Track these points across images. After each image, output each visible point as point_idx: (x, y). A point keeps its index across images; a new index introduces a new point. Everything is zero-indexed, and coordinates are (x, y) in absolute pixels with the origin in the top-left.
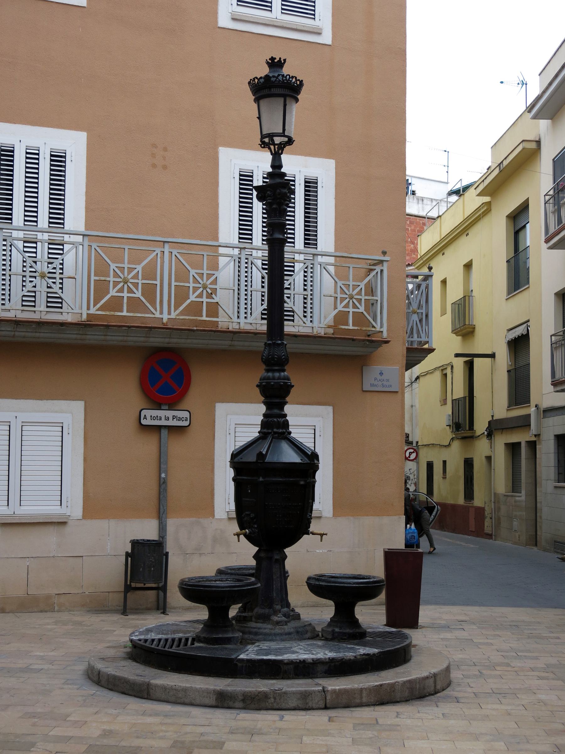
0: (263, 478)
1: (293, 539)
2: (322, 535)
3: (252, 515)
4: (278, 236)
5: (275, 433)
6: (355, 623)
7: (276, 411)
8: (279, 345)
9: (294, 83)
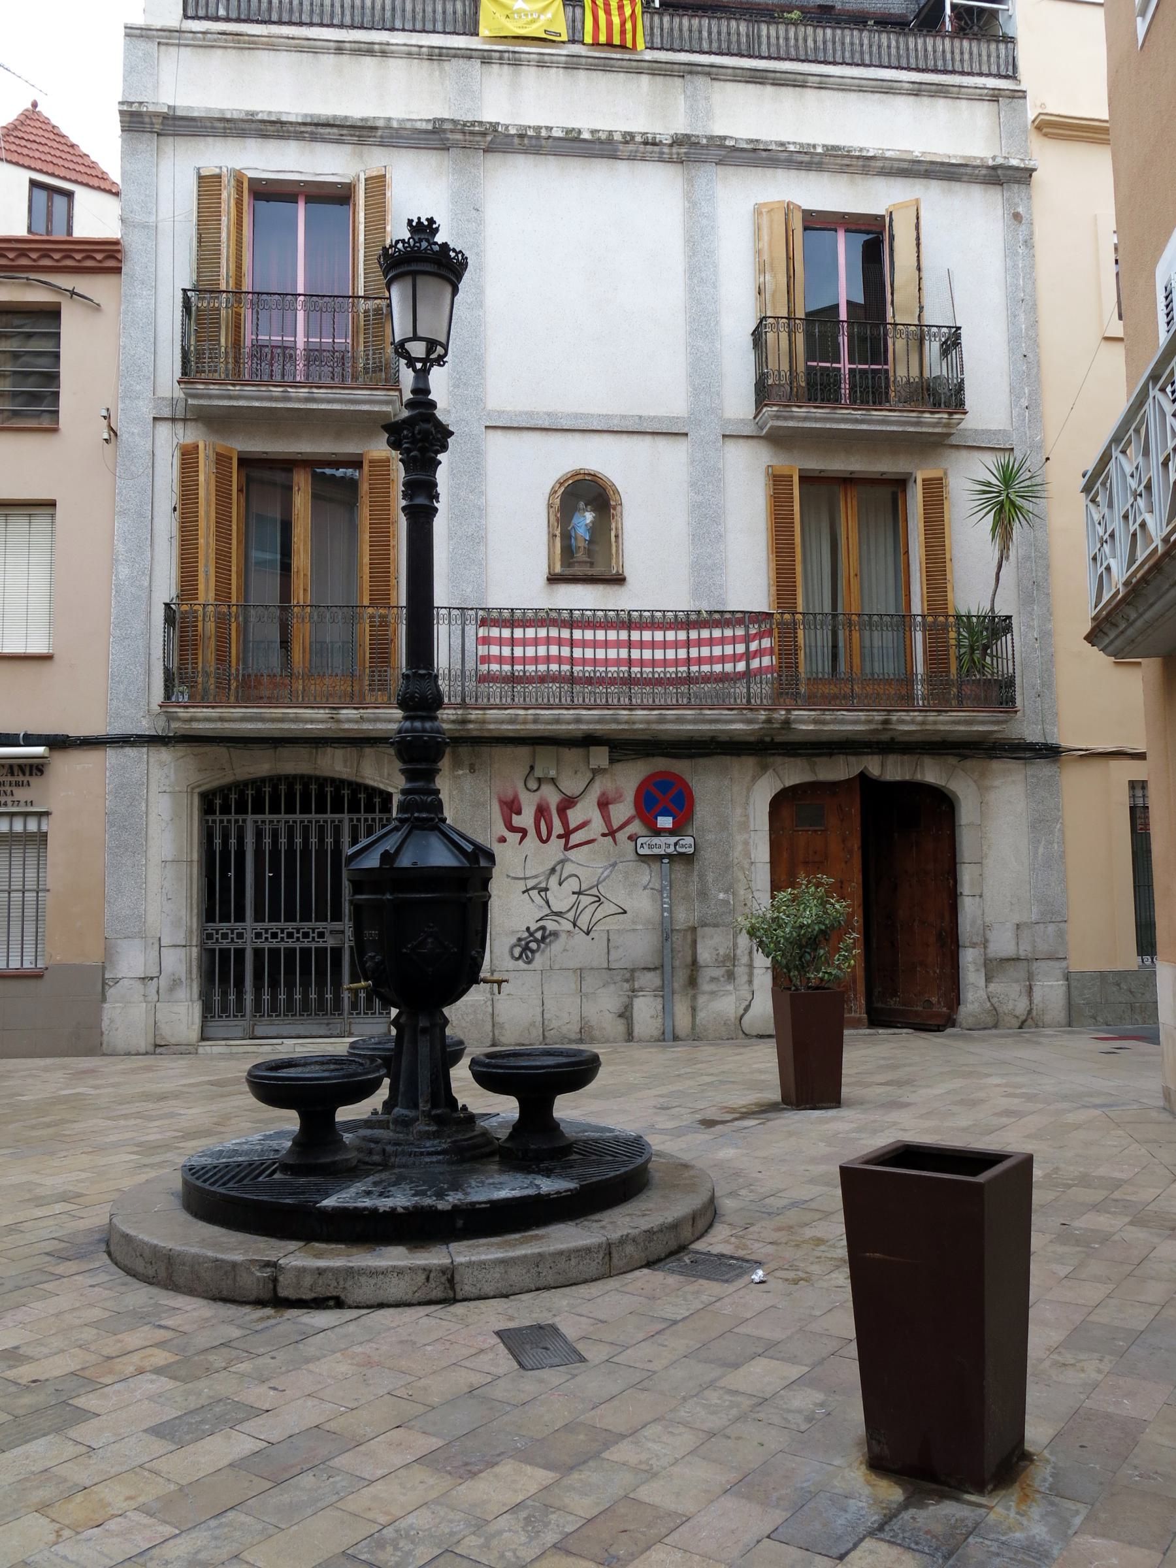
0: (391, 895)
1: (455, 993)
2: (499, 983)
3: (378, 958)
4: (421, 500)
5: (417, 819)
6: (552, 1127)
7: (419, 784)
8: (422, 676)
9: (426, 249)
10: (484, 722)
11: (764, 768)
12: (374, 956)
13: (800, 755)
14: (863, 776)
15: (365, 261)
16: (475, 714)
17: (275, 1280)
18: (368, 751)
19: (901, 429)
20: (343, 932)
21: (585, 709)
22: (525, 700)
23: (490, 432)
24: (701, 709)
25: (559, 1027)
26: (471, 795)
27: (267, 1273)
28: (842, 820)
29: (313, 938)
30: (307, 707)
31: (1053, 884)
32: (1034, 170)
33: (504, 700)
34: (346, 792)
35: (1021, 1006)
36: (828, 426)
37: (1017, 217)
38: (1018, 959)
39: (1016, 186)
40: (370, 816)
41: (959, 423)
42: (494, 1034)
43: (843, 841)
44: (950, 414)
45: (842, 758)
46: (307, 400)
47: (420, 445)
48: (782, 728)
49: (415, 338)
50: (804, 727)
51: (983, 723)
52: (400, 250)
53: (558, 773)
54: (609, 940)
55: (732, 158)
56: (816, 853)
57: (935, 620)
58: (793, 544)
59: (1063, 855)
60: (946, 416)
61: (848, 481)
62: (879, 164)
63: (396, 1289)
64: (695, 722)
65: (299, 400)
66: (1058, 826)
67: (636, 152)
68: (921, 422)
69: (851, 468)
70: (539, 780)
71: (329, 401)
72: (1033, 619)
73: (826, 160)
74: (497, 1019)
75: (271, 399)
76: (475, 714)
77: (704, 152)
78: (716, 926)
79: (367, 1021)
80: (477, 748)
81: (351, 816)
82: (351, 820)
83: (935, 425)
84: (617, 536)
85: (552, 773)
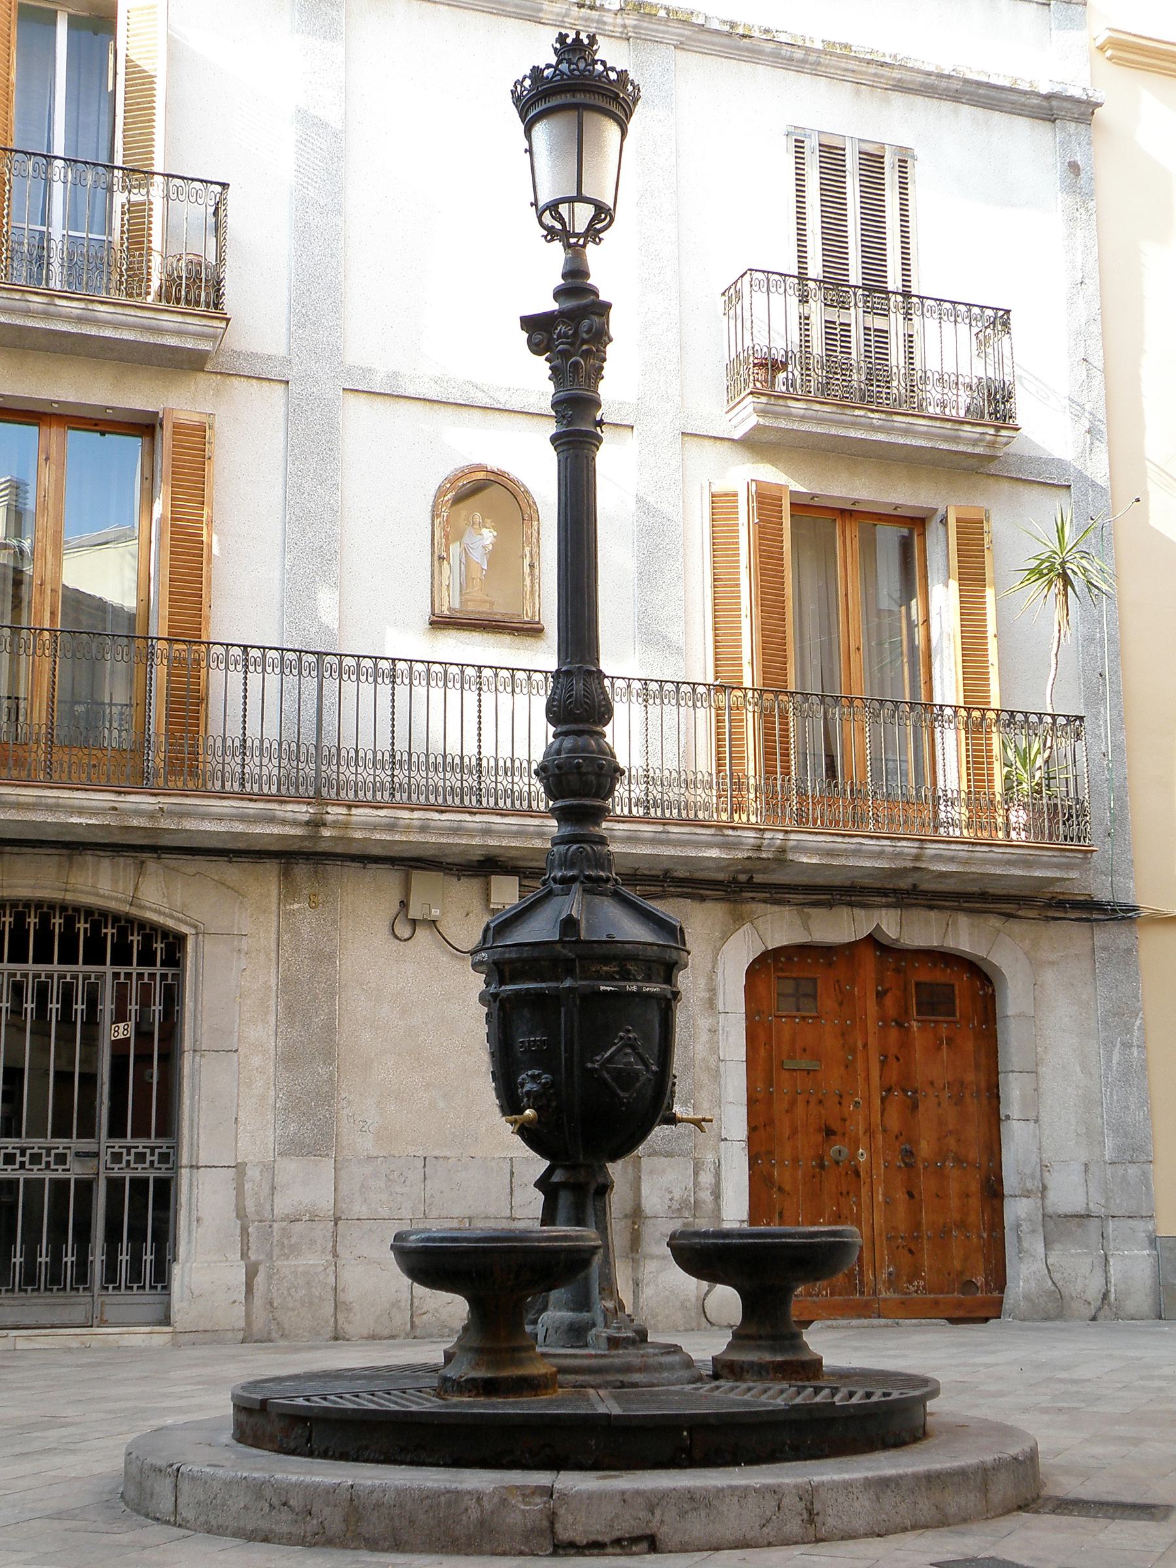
10: (346, 826)
11: (738, 920)
12: (539, 1076)
13: (788, 902)
14: (873, 941)
15: (124, 131)
16: (335, 813)
17: (552, 1517)
18: (152, 866)
19: (930, 445)
20: (97, 1155)
21: (498, 814)
22: (409, 797)
23: (351, 395)
24: (664, 824)
25: (437, 1310)
26: (311, 941)
27: (539, 1503)
28: (841, 1004)
29: (48, 1163)
30: (78, 789)
31: (1133, 1107)
32: (1099, 105)
33: (379, 794)
34: (109, 931)
35: (1094, 1287)
36: (833, 431)
37: (1074, 167)
38: (1089, 1216)
39: (1073, 125)
40: (146, 970)
41: (1007, 444)
42: (336, 1321)
43: (843, 1034)
44: (998, 428)
45: (845, 911)
46: (80, 320)
47: (585, 347)
48: (775, 859)
49: (580, 198)
50: (805, 860)
51: (1048, 866)
52: (562, 73)
53: (443, 914)
54: (512, 1173)
55: (700, 41)
56: (805, 1050)
57: (984, 715)
58: (783, 596)
59: (1144, 1066)
60: (992, 431)
61: (846, 514)
62: (896, 74)
63: (734, 1521)
64: (654, 842)
65: (68, 318)
66: (1138, 1022)
67: (566, 15)
68: (959, 437)
69: (855, 495)
70: (414, 923)
71: (117, 325)
72: (1099, 726)
73: (825, 60)
74: (342, 1296)
75: (27, 313)
76: (335, 813)
77: (662, 28)
78: (669, 1155)
79: (129, 1299)
80: (321, 868)
81: (117, 969)
82: (116, 975)
83: (975, 442)
84: (532, 566)
85: (435, 912)
